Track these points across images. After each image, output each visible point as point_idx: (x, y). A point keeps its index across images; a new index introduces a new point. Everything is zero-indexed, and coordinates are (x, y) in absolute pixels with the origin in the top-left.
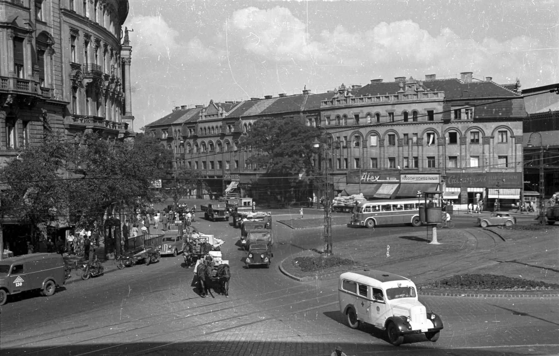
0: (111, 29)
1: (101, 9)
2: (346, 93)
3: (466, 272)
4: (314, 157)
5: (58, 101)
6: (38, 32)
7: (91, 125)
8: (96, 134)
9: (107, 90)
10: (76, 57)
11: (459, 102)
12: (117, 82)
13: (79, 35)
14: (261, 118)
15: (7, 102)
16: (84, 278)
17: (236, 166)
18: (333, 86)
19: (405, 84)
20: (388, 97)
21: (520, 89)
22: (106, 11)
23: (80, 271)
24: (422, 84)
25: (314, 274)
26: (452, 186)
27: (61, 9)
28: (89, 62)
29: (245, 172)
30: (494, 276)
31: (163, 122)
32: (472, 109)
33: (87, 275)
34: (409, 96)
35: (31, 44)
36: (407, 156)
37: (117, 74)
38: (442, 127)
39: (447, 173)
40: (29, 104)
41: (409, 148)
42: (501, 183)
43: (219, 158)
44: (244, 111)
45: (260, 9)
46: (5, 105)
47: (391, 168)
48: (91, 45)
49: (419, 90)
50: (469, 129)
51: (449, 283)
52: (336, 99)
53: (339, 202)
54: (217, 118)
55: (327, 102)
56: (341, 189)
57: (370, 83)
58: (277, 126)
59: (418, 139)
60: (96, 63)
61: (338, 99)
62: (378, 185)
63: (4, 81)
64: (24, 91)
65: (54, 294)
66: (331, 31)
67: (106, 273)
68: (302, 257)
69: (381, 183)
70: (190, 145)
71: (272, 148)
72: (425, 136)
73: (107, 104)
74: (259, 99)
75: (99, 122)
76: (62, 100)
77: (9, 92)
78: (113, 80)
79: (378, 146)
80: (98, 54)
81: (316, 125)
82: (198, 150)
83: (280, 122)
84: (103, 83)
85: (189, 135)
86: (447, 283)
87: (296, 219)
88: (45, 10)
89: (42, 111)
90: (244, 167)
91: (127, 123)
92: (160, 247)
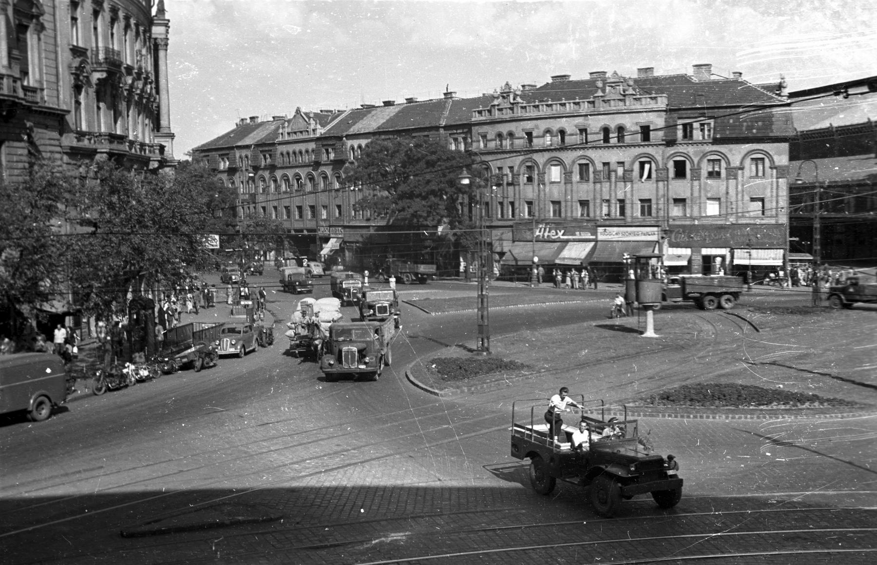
7: (105, 147)
12: (146, 78)
14: (377, 137)
16: (96, 392)
17: (337, 215)
18: (490, 86)
19: (605, 84)
21: (786, 92)
23: (91, 382)
24: (631, 83)
25: (459, 383)
28: (100, 44)
29: (351, 224)
33: (101, 388)
36: (608, 198)
38: (663, 152)
43: (309, 201)
48: (106, 15)
49: (627, 93)
51: (671, 398)
52: (496, 107)
54: (307, 137)
57: (550, 81)
59: (625, 171)
60: (111, 47)
61: (500, 107)
65: (49, 416)
68: (443, 357)
69: (567, 241)
70: (264, 181)
71: (395, 186)
72: (636, 166)
73: (131, 112)
74: (373, 106)
75: (118, 143)
76: (57, 107)
78: (139, 74)
79: (563, 182)
80: (115, 31)
82: (278, 187)
84: (123, 79)
86: (668, 398)
89: (25, 125)
90: (350, 216)
91: (163, 144)
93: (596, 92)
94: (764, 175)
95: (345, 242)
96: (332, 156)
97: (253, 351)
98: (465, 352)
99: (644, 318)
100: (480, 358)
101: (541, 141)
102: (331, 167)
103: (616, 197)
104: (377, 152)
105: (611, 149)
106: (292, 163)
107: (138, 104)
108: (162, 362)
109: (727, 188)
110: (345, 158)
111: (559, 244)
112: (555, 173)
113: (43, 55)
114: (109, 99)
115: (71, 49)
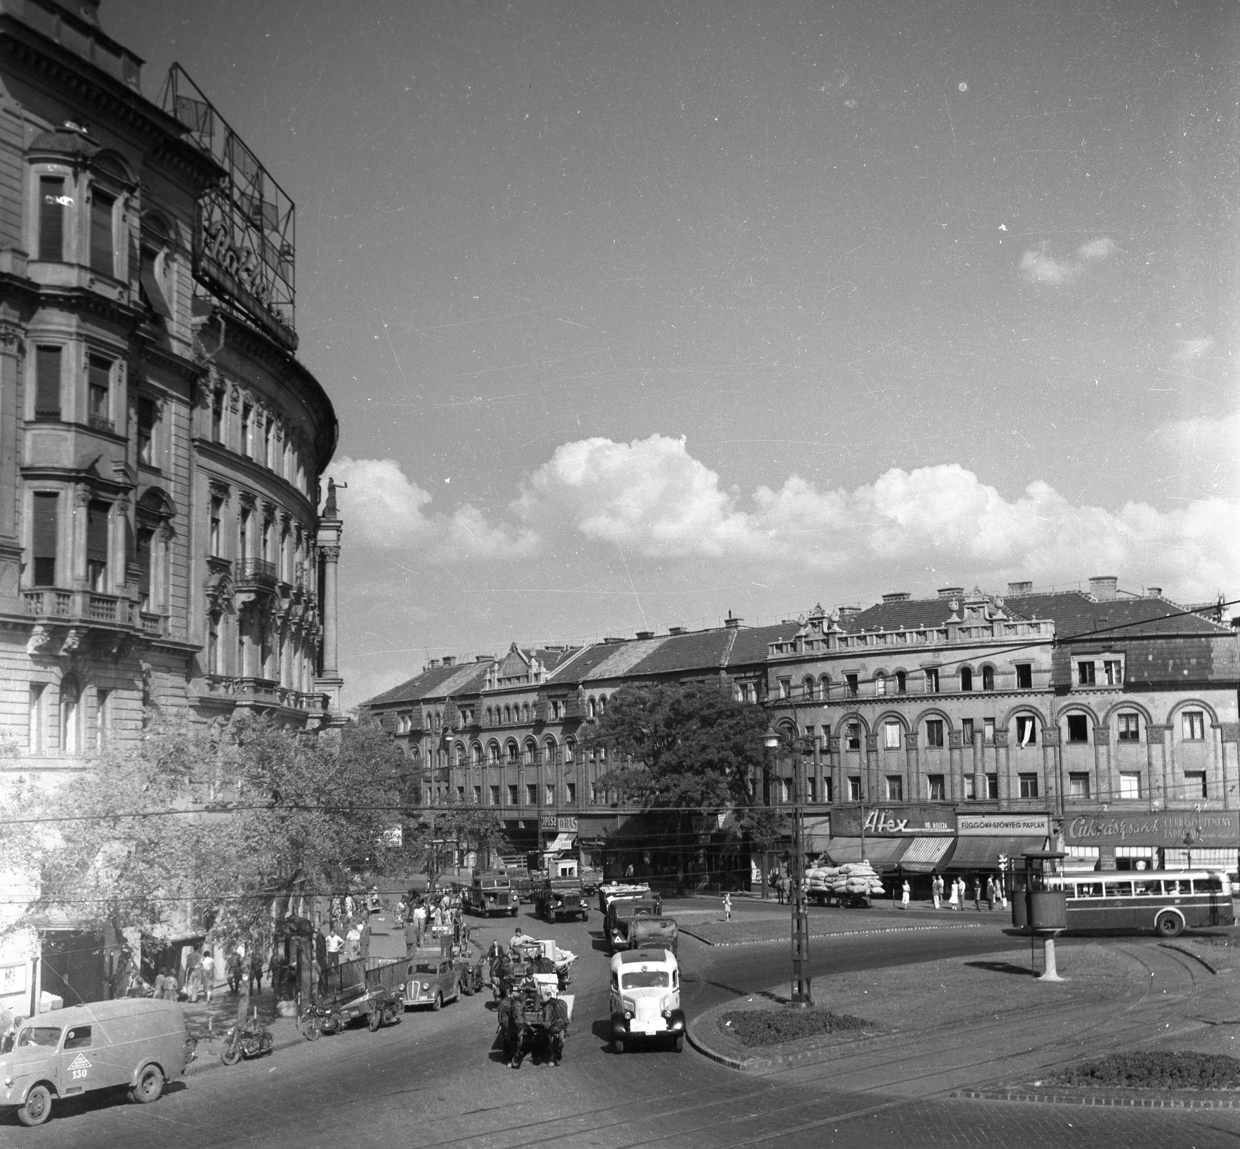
0: (300, 483)
1: (279, 439)
2: (825, 624)
3: (1135, 1047)
4: (755, 774)
5: (176, 644)
6: (141, 490)
7: (247, 697)
8: (263, 718)
9: (285, 619)
10: (221, 545)
11: (1088, 644)
13: (229, 496)
14: (629, 683)
15: (65, 646)
16: (226, 1060)
17: (569, 799)
18: (798, 612)
19: (962, 604)
20: (924, 633)
22: (289, 445)
23: (220, 1044)
24: (1001, 604)
26: (1079, 843)
27: (193, 440)
28: (249, 555)
30: (1204, 1055)
31: (400, 695)
32: (1119, 661)
33: (234, 1054)
34: (973, 630)
35: (126, 516)
37: (309, 584)
39: (1068, 812)
40: (115, 651)
41: (975, 753)
42: (1194, 835)
43: (528, 777)
44: (587, 669)
45: (614, 441)
46: (62, 653)
47: (935, 801)
49: (994, 617)
50: (1114, 707)
51: (1098, 1074)
52: (803, 639)
53: (814, 881)
54: (525, 684)
55: (781, 645)
56: (816, 849)
57: (881, 601)
58: (666, 702)
59: (995, 731)
60: (262, 558)
61: (809, 639)
62: (906, 840)
63: (61, 600)
64: (104, 620)
65: (158, 1098)
66: (777, 485)
67: (280, 1048)
69: (912, 837)
72: (1013, 724)
73: (284, 650)
74: (623, 640)
76: (185, 642)
77: (70, 624)
78: (299, 595)
80: (268, 536)
81: (758, 700)
82: (482, 759)
83: (673, 692)
84: (276, 602)
85: (461, 724)
86: (1092, 1073)
87: (714, 923)
88: (159, 443)
89: (140, 666)
90: (587, 798)
91: (328, 694)
92: (402, 987)
93: (950, 617)
94: (1203, 737)
95: (580, 840)
96: (562, 712)
97: (454, 1000)
98: (771, 1003)
99: (1042, 950)
100: (797, 1011)
101: (870, 686)
102: (560, 729)
103: (983, 770)
104: (628, 706)
105: (974, 699)
106: (503, 723)
107: (296, 637)
108: (322, 1016)
109: (1149, 756)
110: (582, 714)
111: (900, 840)
112: (892, 735)
113: (171, 570)
114: (256, 629)
115: (208, 562)
